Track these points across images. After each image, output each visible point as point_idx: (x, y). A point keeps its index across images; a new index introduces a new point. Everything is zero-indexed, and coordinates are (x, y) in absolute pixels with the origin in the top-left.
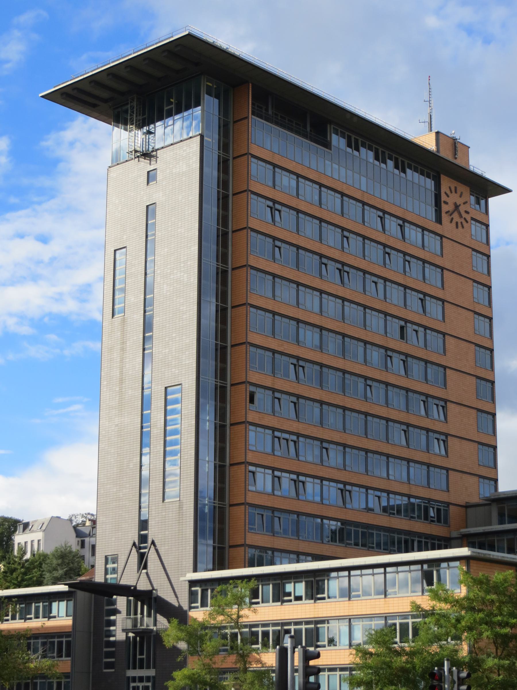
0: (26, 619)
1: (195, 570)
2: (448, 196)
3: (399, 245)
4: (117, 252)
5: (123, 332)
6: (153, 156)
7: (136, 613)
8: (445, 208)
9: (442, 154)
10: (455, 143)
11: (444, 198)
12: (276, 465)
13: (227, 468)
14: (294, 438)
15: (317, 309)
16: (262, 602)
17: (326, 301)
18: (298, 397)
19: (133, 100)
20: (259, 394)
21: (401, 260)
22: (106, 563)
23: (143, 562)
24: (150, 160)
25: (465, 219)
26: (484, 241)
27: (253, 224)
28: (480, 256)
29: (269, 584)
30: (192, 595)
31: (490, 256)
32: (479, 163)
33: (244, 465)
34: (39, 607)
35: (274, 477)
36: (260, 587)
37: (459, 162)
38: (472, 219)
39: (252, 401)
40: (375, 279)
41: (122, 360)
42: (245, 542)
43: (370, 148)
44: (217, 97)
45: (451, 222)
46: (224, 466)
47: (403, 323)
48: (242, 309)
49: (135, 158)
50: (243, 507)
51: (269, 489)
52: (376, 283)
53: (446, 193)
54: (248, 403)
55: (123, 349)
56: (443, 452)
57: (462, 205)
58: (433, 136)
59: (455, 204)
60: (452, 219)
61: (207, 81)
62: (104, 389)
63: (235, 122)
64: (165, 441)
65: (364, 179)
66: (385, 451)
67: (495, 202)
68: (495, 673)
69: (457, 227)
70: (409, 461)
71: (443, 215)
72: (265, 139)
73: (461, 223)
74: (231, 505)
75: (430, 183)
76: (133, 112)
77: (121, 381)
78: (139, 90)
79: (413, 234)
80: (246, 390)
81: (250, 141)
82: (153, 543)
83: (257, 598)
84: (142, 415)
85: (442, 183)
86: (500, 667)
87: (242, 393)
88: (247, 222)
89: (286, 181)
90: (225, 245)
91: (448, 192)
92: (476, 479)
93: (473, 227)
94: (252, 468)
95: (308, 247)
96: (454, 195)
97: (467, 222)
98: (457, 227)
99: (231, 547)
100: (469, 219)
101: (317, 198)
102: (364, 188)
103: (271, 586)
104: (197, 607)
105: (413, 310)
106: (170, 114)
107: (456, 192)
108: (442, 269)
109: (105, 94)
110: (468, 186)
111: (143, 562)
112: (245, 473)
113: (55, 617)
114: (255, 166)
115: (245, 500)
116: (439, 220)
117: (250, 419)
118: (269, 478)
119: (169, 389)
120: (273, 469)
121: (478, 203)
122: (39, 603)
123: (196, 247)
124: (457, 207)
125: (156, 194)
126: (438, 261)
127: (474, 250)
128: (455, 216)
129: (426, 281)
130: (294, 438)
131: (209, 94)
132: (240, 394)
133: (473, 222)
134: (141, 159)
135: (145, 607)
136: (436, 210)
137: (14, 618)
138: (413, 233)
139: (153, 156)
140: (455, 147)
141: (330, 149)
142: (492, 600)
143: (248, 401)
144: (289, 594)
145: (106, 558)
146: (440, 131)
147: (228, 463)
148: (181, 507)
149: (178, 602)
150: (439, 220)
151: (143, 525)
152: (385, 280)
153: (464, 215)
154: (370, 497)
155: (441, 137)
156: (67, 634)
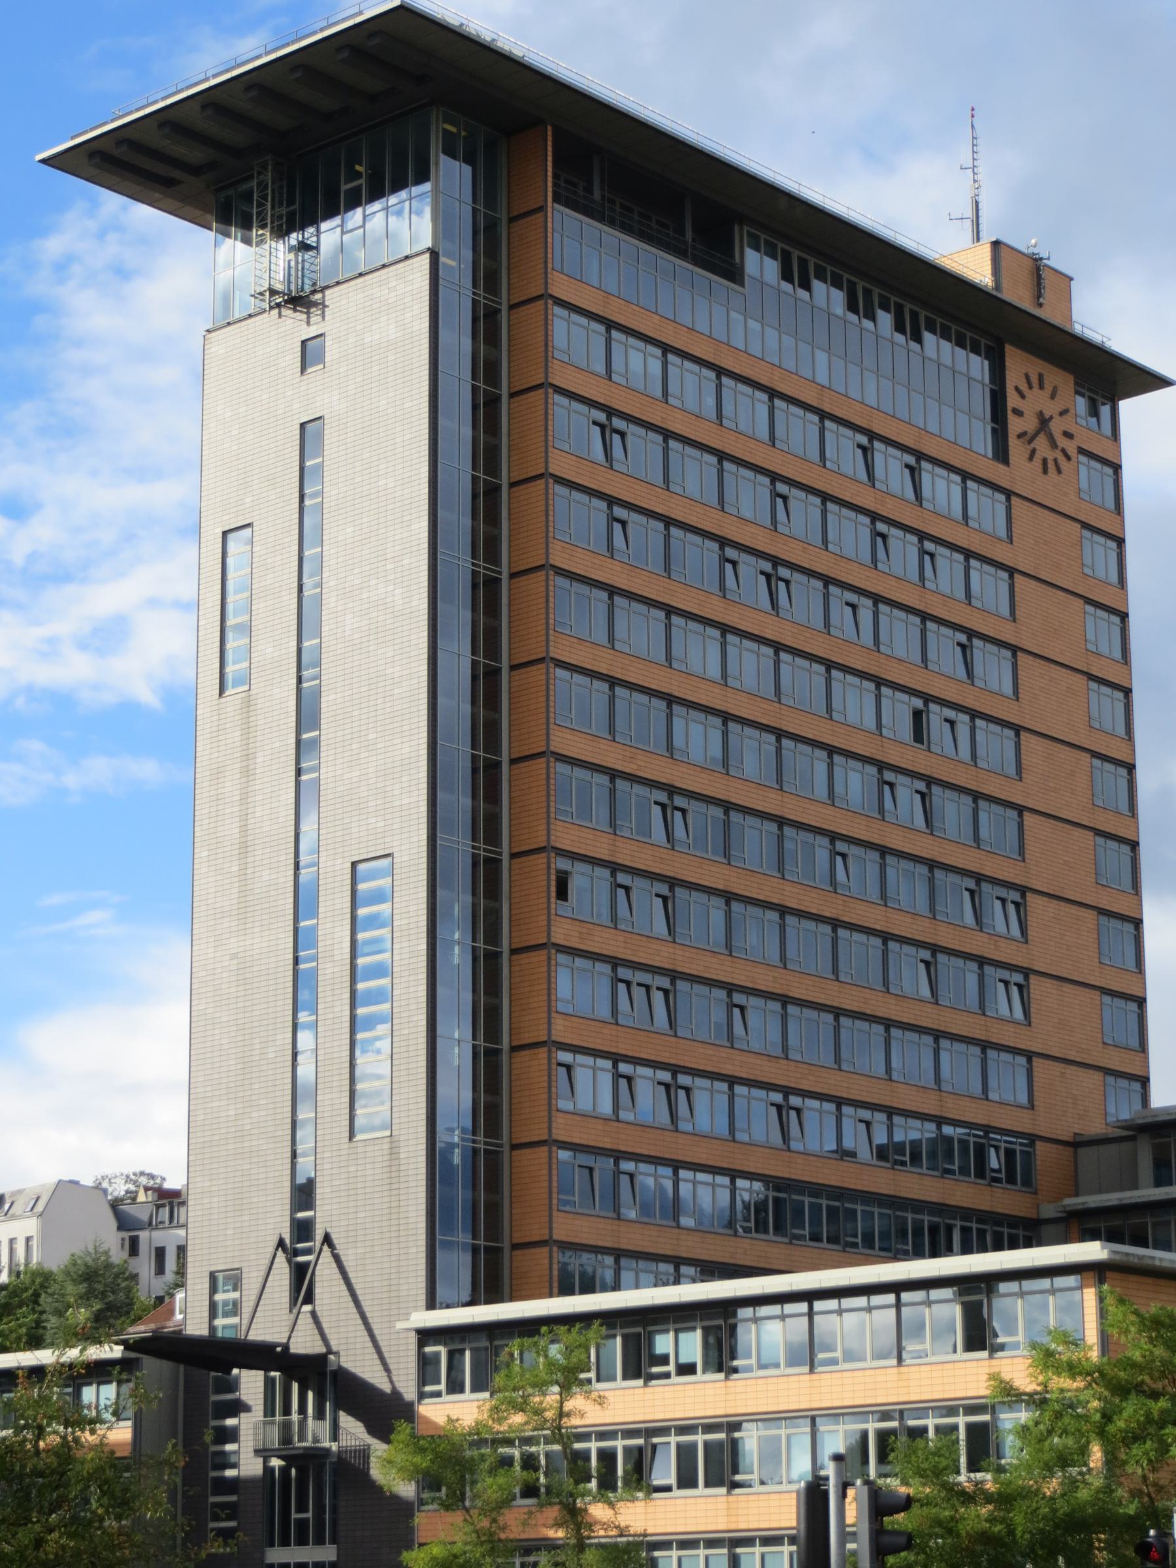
1: (431, 1304)
2: (1023, 396)
4: (230, 536)
6: (315, 304)
7: (287, 1411)
8: (1015, 425)
9: (1007, 295)
10: (1038, 269)
11: (1012, 400)
12: (622, 1049)
14: (665, 982)
21: (913, 552)
22: (213, 1289)
23: (302, 1285)
24: (308, 313)
25: (1064, 451)
27: (560, 465)
29: (614, 1336)
30: (426, 1366)
35: (617, 1076)
37: (1057, 320)
38: (1081, 451)
39: (562, 894)
41: (244, 798)
43: (837, 283)
45: (1031, 458)
47: (918, 703)
49: (271, 308)
51: (606, 1107)
52: (854, 607)
53: (1017, 389)
54: (553, 900)
56: (1018, 1014)
57: (1056, 417)
58: (985, 252)
59: (1041, 414)
60: (1034, 451)
61: (444, 122)
62: (201, 869)
64: (353, 992)
69: (1045, 471)
70: (938, 1035)
71: (1013, 441)
72: (585, 255)
73: (1055, 460)
74: (514, 1147)
75: (978, 367)
76: (265, 197)
77: (244, 849)
79: (941, 489)
80: (549, 868)
81: (550, 265)
82: (327, 1239)
89: (639, 363)
90: (493, 795)
91: (1024, 387)
92: (1097, 1076)
93: (1083, 470)
94: (565, 1057)
95: (692, 520)
96: (1038, 392)
97: (1069, 458)
98: (1045, 471)
99: (515, 1247)
100: (1072, 451)
101: (711, 401)
103: (619, 1340)
106: (354, 201)
107: (1041, 387)
111: (302, 1285)
112: (550, 1069)
116: (1001, 454)
117: (558, 937)
118: (605, 1080)
120: (616, 1058)
121: (1094, 412)
124: (1044, 422)
125: (320, 395)
128: (1041, 443)
131: (450, 152)
134: (285, 312)
136: (994, 431)
139: (315, 304)
140: (1039, 277)
141: (742, 285)
143: (553, 894)
144: (664, 1359)
145: (213, 1277)
148: (394, 1151)
149: (391, 1382)
150: (1001, 454)
152: (877, 599)
153: (1062, 442)
154: (847, 1124)
155: (1004, 253)
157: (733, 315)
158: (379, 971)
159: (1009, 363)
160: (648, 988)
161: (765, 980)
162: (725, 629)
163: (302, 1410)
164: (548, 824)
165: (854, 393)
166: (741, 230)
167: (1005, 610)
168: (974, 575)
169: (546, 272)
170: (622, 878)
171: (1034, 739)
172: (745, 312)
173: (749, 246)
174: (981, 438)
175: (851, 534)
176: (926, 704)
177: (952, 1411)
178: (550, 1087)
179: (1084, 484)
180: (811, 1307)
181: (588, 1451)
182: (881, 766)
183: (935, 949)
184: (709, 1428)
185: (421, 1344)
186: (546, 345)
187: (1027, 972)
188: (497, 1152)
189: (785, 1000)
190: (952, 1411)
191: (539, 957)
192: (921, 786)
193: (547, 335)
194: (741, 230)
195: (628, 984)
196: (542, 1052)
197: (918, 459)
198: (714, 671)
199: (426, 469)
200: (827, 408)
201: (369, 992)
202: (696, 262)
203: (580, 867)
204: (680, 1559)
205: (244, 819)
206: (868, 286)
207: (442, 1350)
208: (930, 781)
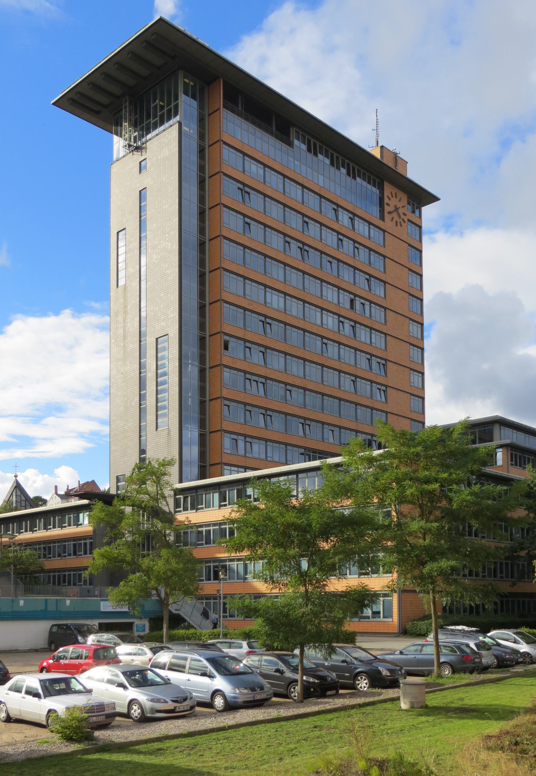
0: (62, 527)
2: (390, 199)
3: (350, 234)
4: (120, 233)
5: (125, 298)
6: (144, 148)
8: (387, 209)
9: (385, 161)
10: (396, 157)
11: (386, 200)
12: (247, 401)
13: (207, 402)
15: (281, 278)
16: (229, 505)
17: (289, 272)
18: (266, 347)
19: (126, 101)
20: (233, 343)
21: (351, 246)
24: (141, 152)
25: (403, 220)
26: (420, 386)
28: (417, 398)
29: (234, 490)
31: (423, 324)
32: (415, 174)
33: (220, 400)
34: (70, 517)
36: (227, 492)
37: (402, 173)
38: (409, 220)
39: (226, 348)
40: (330, 259)
42: (222, 460)
45: (392, 220)
49: (130, 152)
50: (220, 433)
52: (331, 263)
53: (388, 196)
54: (223, 350)
55: (125, 312)
56: (383, 399)
57: (401, 208)
58: (379, 149)
59: (396, 206)
60: (393, 218)
61: (184, 78)
63: (209, 115)
64: (157, 382)
68: (420, 538)
69: (397, 225)
70: (356, 404)
71: (386, 214)
72: (235, 128)
73: (400, 222)
74: (210, 433)
75: (376, 191)
76: (126, 112)
77: (125, 337)
80: (221, 339)
81: (222, 129)
83: (225, 501)
84: (140, 363)
85: (385, 188)
86: (425, 532)
87: (218, 341)
88: (220, 199)
89: (254, 168)
91: (390, 196)
92: (409, 421)
93: (409, 227)
95: (274, 226)
96: (395, 200)
97: (405, 222)
98: (397, 225)
99: (211, 465)
100: (406, 220)
101: (281, 186)
102: (321, 184)
103: (235, 490)
104: (180, 511)
107: (396, 197)
108: (385, 257)
109: (105, 100)
110: (406, 194)
112: (221, 406)
113: (81, 525)
115: (221, 427)
116: (382, 218)
119: (159, 340)
121: (413, 212)
122: (71, 514)
123: (177, 219)
124: (396, 209)
126: (381, 250)
127: (410, 245)
128: (395, 215)
129: (372, 265)
132: (217, 342)
133: (409, 223)
134: (135, 153)
136: (380, 210)
137: (54, 527)
138: (361, 225)
139: (144, 148)
140: (396, 159)
141: (293, 148)
142: (417, 453)
143: (223, 348)
144: (250, 497)
145: (117, 477)
146: (384, 145)
148: (169, 433)
149: (169, 509)
150: (382, 218)
154: (325, 431)
155: (384, 150)
156: (90, 537)
157: (290, 158)
159: (385, 187)
160: (257, 382)
163: (143, 516)
164: (221, 324)
165: (332, 190)
166: (293, 130)
167: (382, 270)
168: (372, 257)
169: (220, 132)
171: (391, 312)
173: (296, 139)
174: (375, 210)
175: (331, 239)
176: (355, 297)
178: (221, 412)
179: (409, 231)
180: (297, 477)
181: (226, 528)
185: (175, 495)
186: (220, 158)
187: (387, 386)
188: (205, 434)
191: (218, 369)
192: (353, 324)
193: (220, 154)
194: (293, 130)
195: (250, 380)
197: (353, 216)
199: (177, 200)
201: (161, 382)
202: (277, 137)
203: (232, 339)
204: (237, 564)
205: (124, 328)
206: (338, 155)
207: (182, 497)
208: (356, 322)
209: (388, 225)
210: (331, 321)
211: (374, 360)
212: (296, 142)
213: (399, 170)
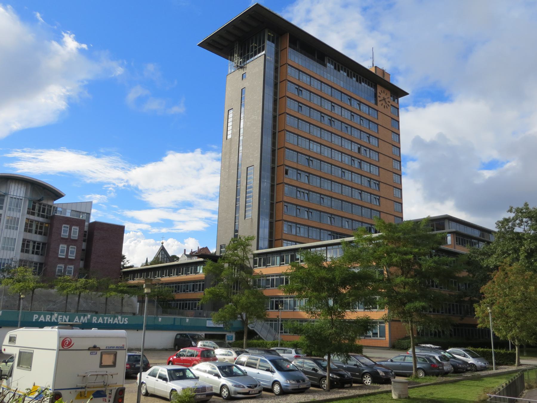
8: (379, 99)
9: (377, 74)
11: (378, 94)
14: (307, 192)
20: (290, 171)
27: (288, 94)
30: (255, 263)
38: (391, 105)
39: (287, 173)
43: (345, 71)
44: (273, 42)
46: (273, 203)
47: (359, 146)
48: (283, 132)
56: (378, 204)
63: (281, 51)
64: (246, 192)
65: (342, 83)
66: (351, 201)
67: (401, 100)
72: (295, 58)
77: (229, 166)
78: (238, 39)
79: (364, 108)
86: (405, 284)
87: (282, 170)
89: (305, 78)
95: (366, 206)
96: (383, 94)
101: (319, 87)
105: (365, 140)
108: (378, 125)
114: (290, 70)
116: (376, 104)
117: (285, 181)
121: (394, 101)
125: (246, 83)
130: (307, 192)
131: (269, 40)
135: (9, 155)
144: (298, 259)
147: (275, 202)
148: (252, 221)
150: (376, 104)
151: (236, 231)
152: (352, 126)
153: (388, 103)
156: (202, 281)
158: (251, 187)
161: (328, 193)
162: (321, 128)
170: (322, 196)
172: (327, 72)
174: (373, 101)
177: (273, 276)
182: (352, 156)
183: (362, 191)
184: (277, 276)
189: (332, 197)
190: (273, 276)
196: (281, 203)
198: (319, 136)
200: (342, 91)
202: (317, 62)
208: (361, 160)
209: (380, 107)
210: (347, 159)
211: (372, 181)
212: (328, 65)
213: (386, 78)
